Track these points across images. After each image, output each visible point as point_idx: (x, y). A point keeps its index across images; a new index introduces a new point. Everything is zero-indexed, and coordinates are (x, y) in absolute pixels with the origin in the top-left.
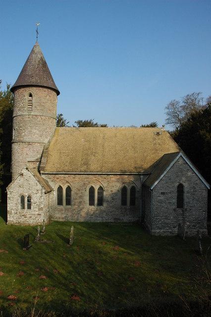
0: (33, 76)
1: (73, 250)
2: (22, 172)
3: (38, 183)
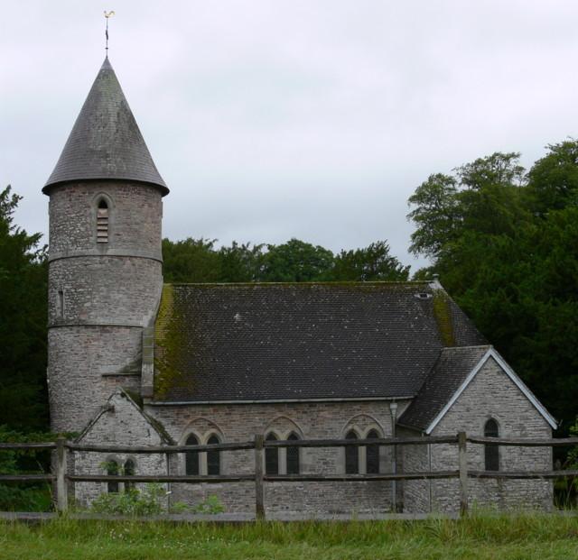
0: (107, 156)
1: (465, 446)
2: (112, 403)
3: (152, 430)
